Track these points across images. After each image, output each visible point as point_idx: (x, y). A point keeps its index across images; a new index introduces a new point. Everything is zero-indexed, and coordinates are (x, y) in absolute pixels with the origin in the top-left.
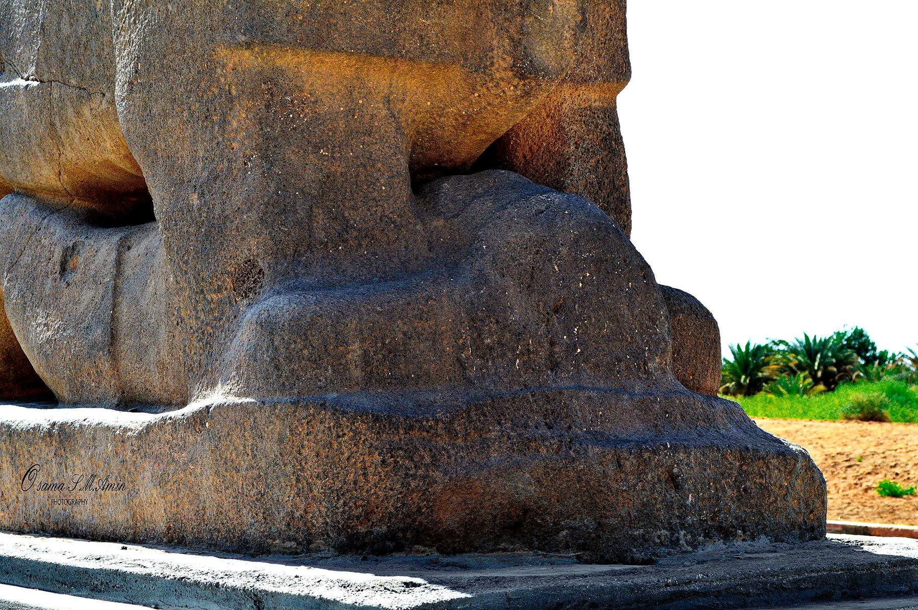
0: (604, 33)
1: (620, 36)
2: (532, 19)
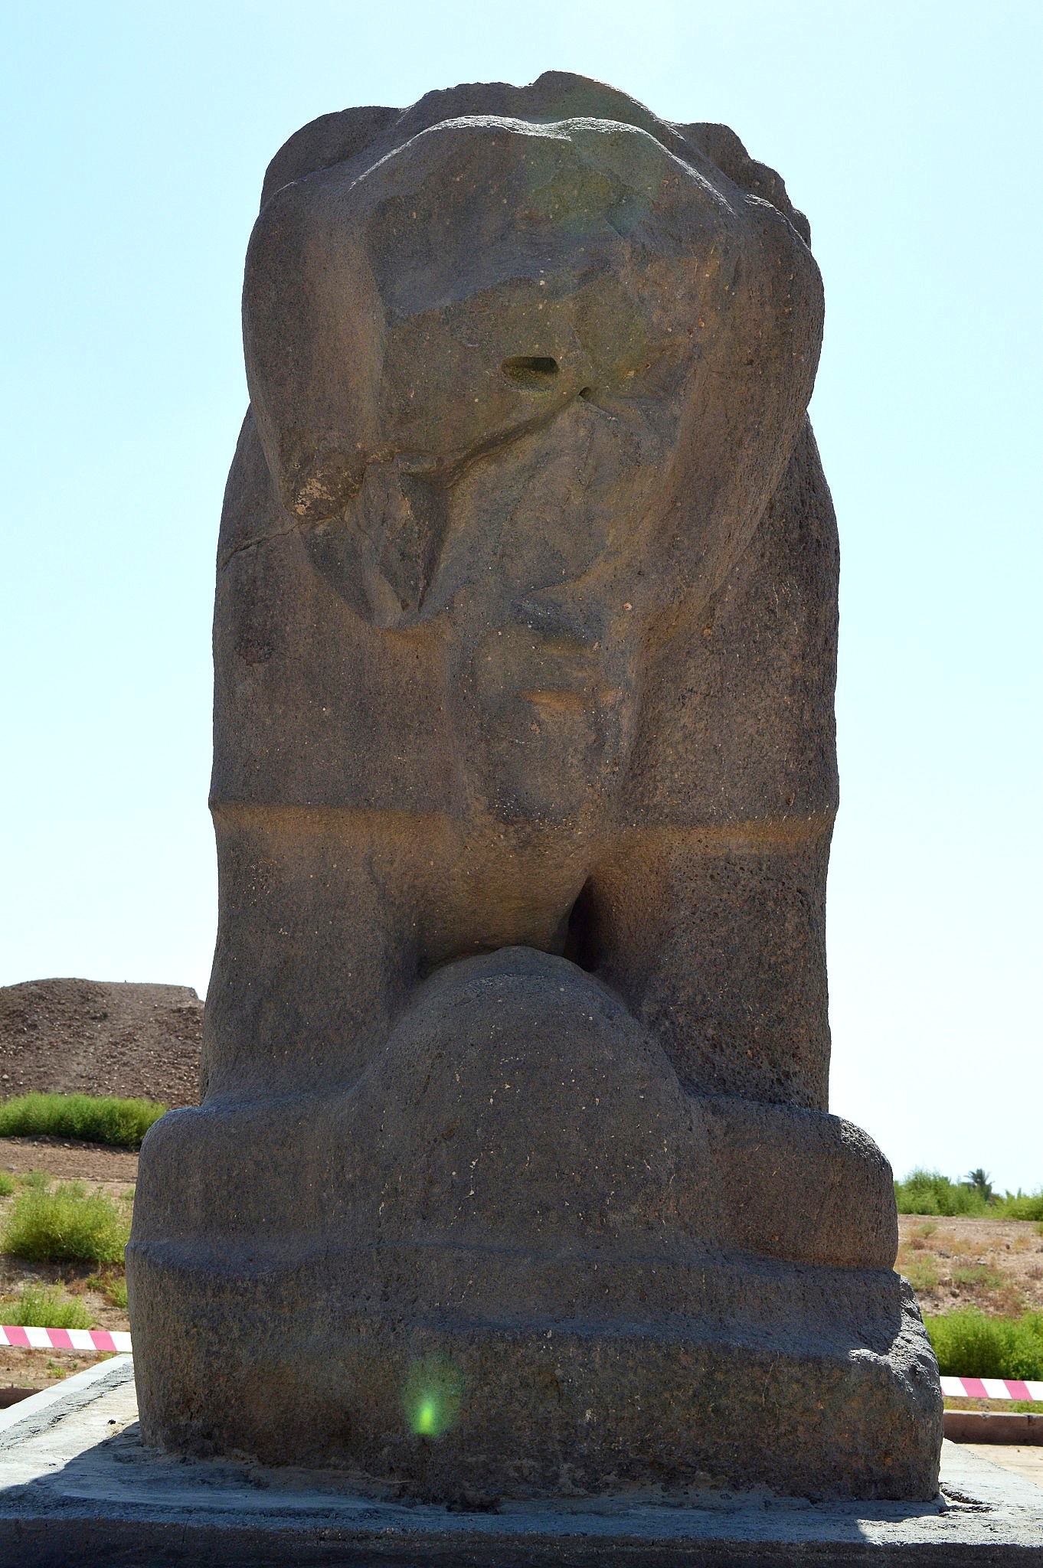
2: (504, 744)
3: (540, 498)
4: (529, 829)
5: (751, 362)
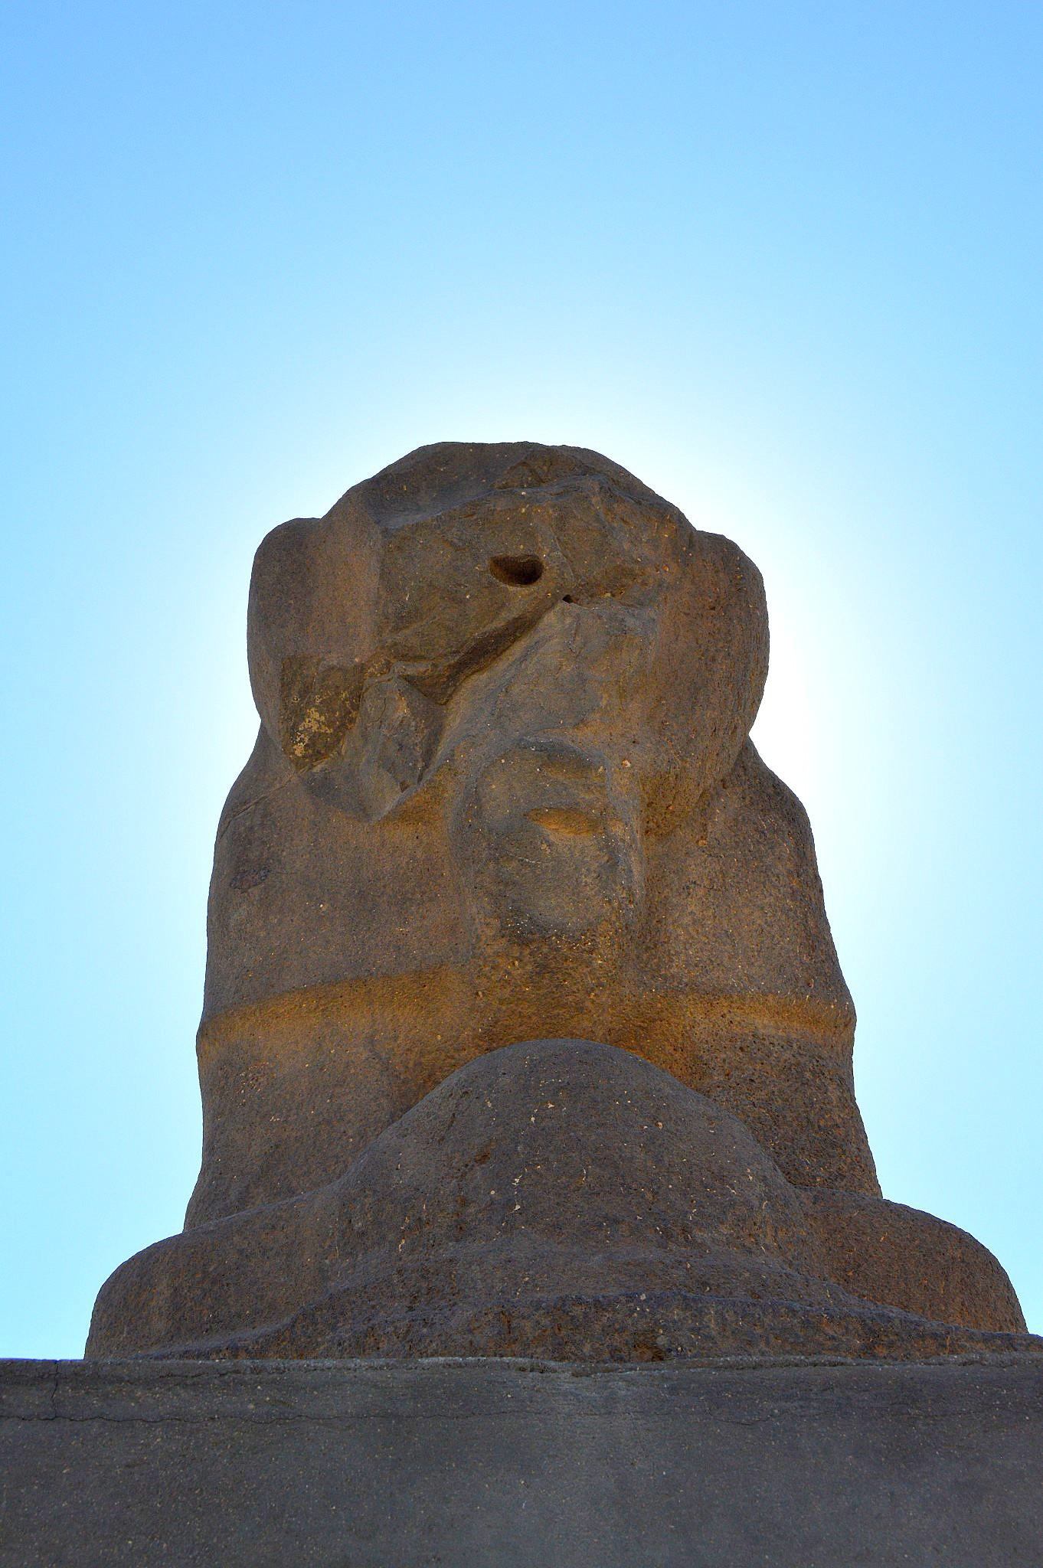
4: (545, 950)
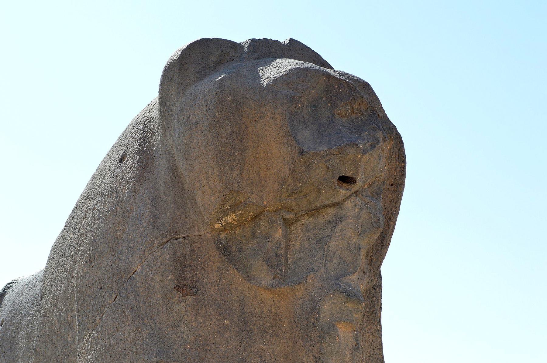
0: (369, 351)
1: (379, 352)
2: (326, 345)
3: (339, 236)
5: (392, 185)
